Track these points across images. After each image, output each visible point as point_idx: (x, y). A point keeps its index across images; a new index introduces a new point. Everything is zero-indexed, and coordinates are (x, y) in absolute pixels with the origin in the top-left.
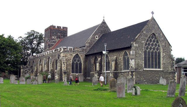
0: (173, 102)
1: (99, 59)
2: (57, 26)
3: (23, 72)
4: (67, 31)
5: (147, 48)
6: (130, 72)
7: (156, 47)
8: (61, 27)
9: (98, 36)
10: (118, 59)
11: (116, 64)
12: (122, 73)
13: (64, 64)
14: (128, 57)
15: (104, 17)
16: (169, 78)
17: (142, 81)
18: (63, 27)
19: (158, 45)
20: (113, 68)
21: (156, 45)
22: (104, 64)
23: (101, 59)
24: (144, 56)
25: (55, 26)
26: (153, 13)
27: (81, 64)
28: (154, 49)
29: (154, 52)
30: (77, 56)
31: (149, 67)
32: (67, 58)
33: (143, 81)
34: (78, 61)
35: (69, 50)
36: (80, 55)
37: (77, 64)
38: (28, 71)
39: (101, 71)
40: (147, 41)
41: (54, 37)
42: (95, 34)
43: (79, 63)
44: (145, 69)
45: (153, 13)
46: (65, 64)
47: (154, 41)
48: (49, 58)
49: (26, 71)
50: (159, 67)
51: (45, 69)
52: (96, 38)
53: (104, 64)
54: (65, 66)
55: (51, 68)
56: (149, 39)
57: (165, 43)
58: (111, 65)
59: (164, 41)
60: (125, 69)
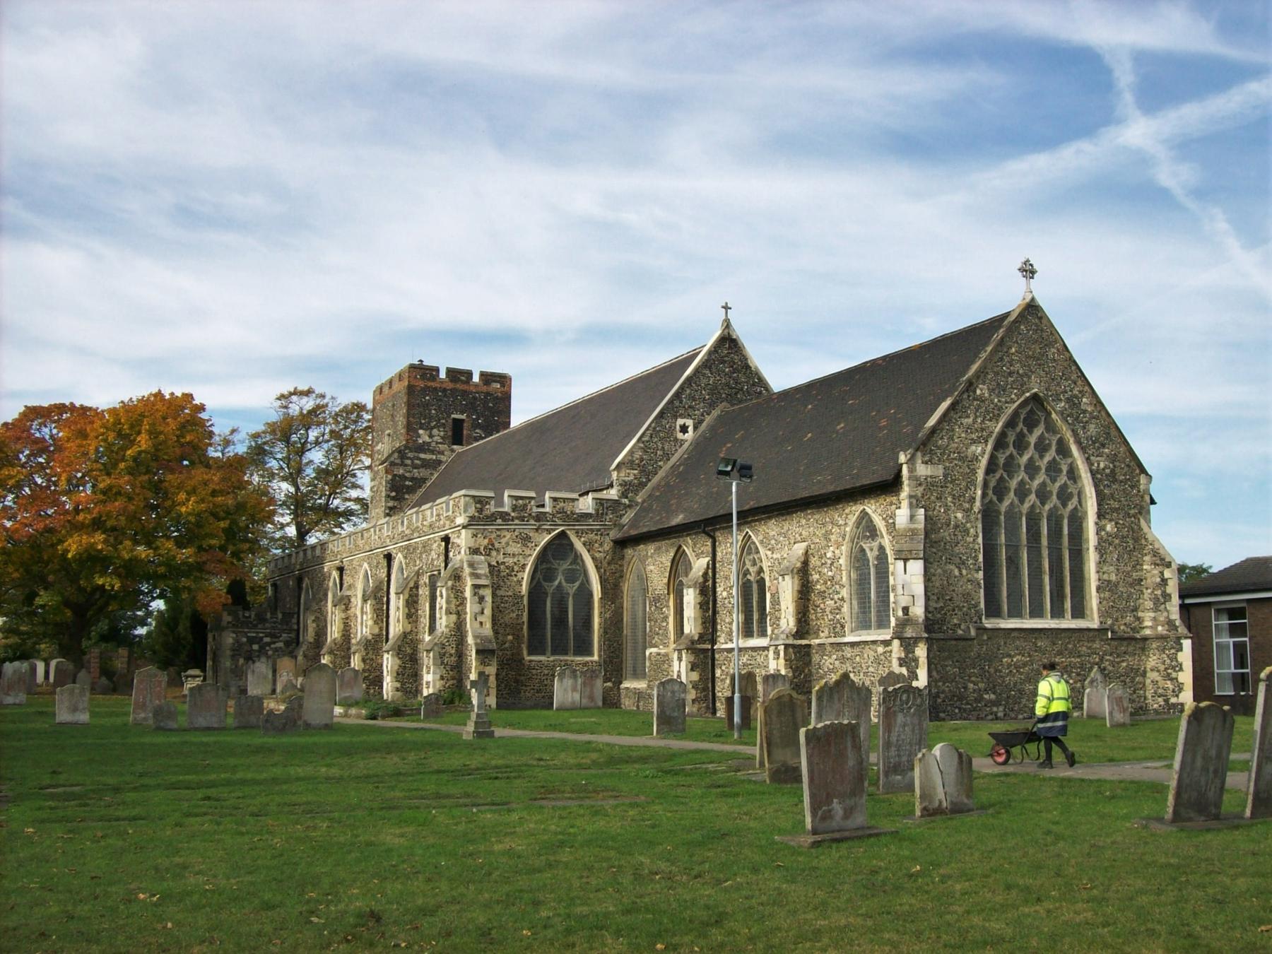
1: (699, 564)
3: (237, 651)
4: (506, 398)
6: (896, 643)
7: (1054, 481)
9: (689, 422)
10: (814, 561)
11: (805, 593)
12: (848, 652)
14: (881, 548)
16: (1144, 674)
17: (976, 700)
18: (483, 374)
19: (1065, 468)
20: (788, 621)
21: (1053, 469)
22: (728, 592)
23: (713, 565)
24: (980, 540)
25: (437, 370)
26: (1028, 271)
27: (585, 594)
28: (1043, 495)
29: (1024, 512)
30: (560, 546)
32: (496, 558)
33: (982, 698)
34: (571, 577)
35: (514, 508)
36: (578, 545)
38: (267, 640)
39: (714, 642)
40: (1000, 444)
41: (431, 436)
42: (671, 411)
43: (572, 589)
44: (989, 623)
46: (489, 599)
48: (389, 558)
49: (251, 641)
50: (1079, 611)
51: (364, 627)
52: (680, 436)
53: (728, 592)
54: (488, 612)
55: (396, 627)
56: (1011, 438)
57: (1113, 458)
58: (776, 602)
59: (1103, 446)
60: (864, 625)
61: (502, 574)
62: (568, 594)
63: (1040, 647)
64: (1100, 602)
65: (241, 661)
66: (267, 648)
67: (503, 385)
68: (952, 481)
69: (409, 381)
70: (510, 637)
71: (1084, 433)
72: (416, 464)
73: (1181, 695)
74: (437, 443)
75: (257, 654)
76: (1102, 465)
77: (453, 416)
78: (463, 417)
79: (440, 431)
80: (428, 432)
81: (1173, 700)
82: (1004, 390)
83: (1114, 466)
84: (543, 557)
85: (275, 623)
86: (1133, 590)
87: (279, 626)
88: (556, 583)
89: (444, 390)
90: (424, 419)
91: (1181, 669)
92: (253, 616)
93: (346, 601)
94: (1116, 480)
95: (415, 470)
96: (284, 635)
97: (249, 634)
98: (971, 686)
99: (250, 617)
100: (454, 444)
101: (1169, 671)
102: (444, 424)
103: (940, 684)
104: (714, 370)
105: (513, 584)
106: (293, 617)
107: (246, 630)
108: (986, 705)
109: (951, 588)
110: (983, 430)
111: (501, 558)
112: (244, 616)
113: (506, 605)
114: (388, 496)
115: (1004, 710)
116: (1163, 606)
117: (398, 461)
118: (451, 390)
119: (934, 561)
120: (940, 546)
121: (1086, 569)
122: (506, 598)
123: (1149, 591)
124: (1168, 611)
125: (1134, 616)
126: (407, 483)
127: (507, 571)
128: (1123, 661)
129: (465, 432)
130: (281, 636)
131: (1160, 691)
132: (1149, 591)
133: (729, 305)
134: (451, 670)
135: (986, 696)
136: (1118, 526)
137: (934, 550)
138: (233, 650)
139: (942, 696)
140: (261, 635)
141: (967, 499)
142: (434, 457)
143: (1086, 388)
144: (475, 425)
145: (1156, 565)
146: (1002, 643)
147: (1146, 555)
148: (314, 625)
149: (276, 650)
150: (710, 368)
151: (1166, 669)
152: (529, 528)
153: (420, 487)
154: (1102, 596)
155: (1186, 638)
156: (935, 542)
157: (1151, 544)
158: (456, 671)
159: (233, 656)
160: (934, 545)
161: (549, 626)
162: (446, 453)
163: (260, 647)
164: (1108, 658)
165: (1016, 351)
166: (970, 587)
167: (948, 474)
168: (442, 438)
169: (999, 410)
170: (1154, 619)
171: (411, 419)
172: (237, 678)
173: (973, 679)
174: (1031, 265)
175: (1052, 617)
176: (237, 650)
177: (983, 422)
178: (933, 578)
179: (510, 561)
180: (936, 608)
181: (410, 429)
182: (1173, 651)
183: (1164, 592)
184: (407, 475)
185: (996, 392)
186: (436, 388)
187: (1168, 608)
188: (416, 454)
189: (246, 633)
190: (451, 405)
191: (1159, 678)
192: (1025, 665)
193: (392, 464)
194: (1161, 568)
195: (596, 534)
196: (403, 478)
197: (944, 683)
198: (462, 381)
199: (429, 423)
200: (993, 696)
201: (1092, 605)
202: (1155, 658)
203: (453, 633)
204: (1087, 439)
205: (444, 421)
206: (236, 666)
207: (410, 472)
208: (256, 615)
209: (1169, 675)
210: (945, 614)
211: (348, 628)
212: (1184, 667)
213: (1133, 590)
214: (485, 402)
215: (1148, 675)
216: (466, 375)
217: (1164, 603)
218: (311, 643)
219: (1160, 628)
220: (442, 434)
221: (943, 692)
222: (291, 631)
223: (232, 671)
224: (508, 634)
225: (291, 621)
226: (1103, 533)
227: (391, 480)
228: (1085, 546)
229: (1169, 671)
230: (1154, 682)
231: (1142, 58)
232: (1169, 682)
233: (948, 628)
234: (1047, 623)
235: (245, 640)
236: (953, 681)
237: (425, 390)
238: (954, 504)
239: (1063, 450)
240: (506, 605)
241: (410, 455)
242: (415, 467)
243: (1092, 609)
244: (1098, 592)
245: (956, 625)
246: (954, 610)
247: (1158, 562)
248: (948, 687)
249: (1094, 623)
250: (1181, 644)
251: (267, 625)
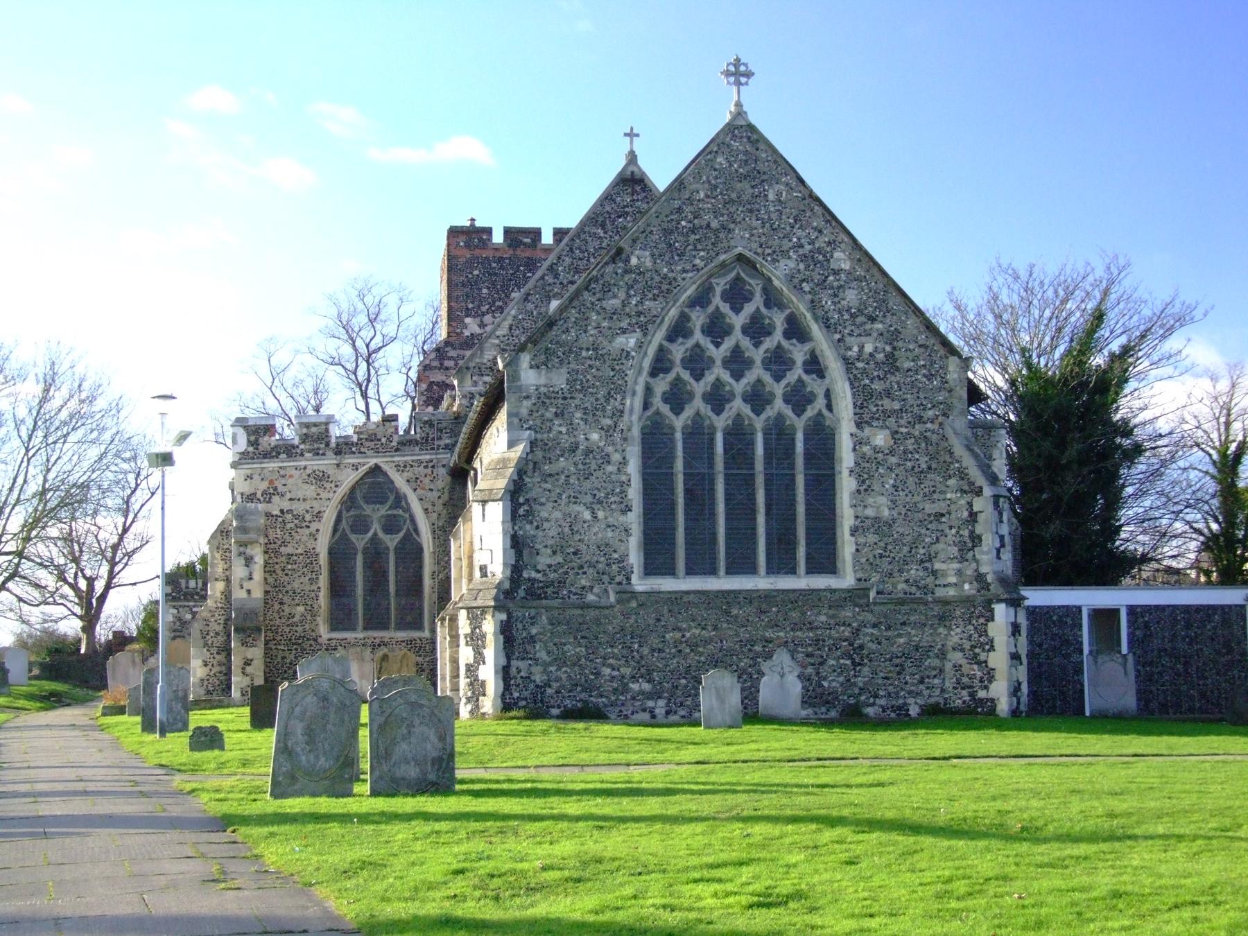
0: (229, 913)
2: (508, 231)
5: (677, 398)
8: (536, 233)
13: (249, 561)
15: (631, 135)
16: (942, 655)
25: (488, 231)
31: (701, 564)
32: (276, 505)
33: (625, 689)
36: (399, 481)
37: (375, 555)
41: (482, 325)
43: (391, 541)
45: (738, 73)
46: (259, 559)
47: (757, 329)
50: (824, 561)
54: (258, 575)
57: (893, 337)
59: (873, 319)
61: (289, 526)
62: (388, 548)
63: (736, 617)
64: (857, 550)
68: (583, 390)
70: (301, 609)
71: (834, 303)
73: (993, 686)
76: (869, 348)
80: (478, 320)
81: (982, 694)
82: (680, 255)
83: (894, 348)
84: (350, 501)
86: (923, 531)
88: (370, 534)
90: (473, 303)
91: (992, 648)
94: (898, 369)
98: (607, 671)
101: (977, 650)
103: (553, 669)
104: (609, 226)
105: (305, 538)
107: (191, 604)
108: (633, 698)
109: (577, 537)
110: (639, 314)
111: (286, 505)
113: (294, 567)
115: (667, 705)
116: (970, 554)
117: (436, 364)
119: (548, 500)
120: (557, 480)
121: (838, 502)
122: (295, 558)
123: (954, 531)
124: (977, 561)
125: (926, 569)
127: (296, 521)
128: (900, 636)
131: (965, 680)
132: (954, 531)
133: (635, 131)
134: (218, 653)
135: (634, 686)
136: (897, 436)
137: (548, 486)
139: (555, 685)
141: (609, 413)
143: (843, 236)
145: (963, 492)
146: (665, 611)
147: (950, 477)
150: (603, 226)
151: (973, 647)
152: (326, 463)
154: (862, 540)
155: (1000, 601)
156: (550, 475)
157: (958, 461)
158: (224, 654)
160: (548, 479)
161: (360, 591)
164: (870, 630)
165: (707, 196)
166: (610, 534)
167: (575, 380)
169: (670, 283)
170: (959, 573)
171: (452, 304)
173: (611, 661)
174: (746, 65)
176: (178, 631)
177: (641, 302)
178: (546, 525)
179: (299, 508)
180: (550, 566)
182: (982, 620)
183: (972, 532)
185: (667, 258)
186: (487, 258)
187: (977, 557)
191: (963, 662)
192: (706, 642)
194: (968, 497)
195: (426, 467)
197: (559, 669)
198: (525, 244)
199: (479, 307)
200: (646, 687)
201: (844, 557)
202: (958, 630)
203: (220, 605)
204: (840, 312)
209: (976, 655)
210: (567, 573)
212: (996, 644)
213: (923, 531)
215: (949, 656)
217: (972, 549)
219: (967, 586)
221: (558, 679)
224: (298, 605)
226: (866, 449)
228: (837, 468)
229: (977, 650)
230: (958, 667)
232: (975, 667)
233: (570, 592)
234: (761, 582)
236: (574, 665)
238: (586, 421)
239: (795, 330)
240: (294, 567)
243: (844, 561)
244: (852, 535)
245: (583, 588)
246: (581, 567)
247: (966, 488)
248: (566, 672)
249: (846, 580)
250: (992, 611)
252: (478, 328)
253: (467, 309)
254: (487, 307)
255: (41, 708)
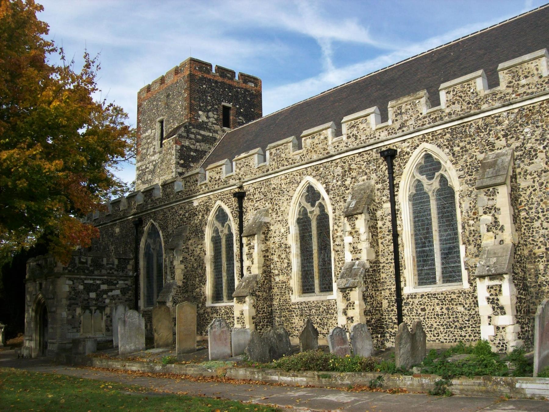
8: (233, 73)
38: (104, 287)
41: (208, 117)
49: (89, 288)
65: (79, 311)
66: (105, 296)
67: (256, 85)
69: (190, 71)
72: (198, 139)
74: (213, 124)
75: (94, 302)
77: (223, 104)
78: (230, 105)
79: (214, 114)
85: (111, 269)
87: (116, 273)
89: (216, 82)
92: (89, 262)
93: (264, 229)
95: (197, 144)
96: (120, 282)
97: (86, 282)
99: (86, 263)
100: (224, 126)
102: (216, 109)
106: (128, 263)
112: (81, 262)
114: (178, 163)
117: (185, 134)
118: (221, 83)
126: (192, 153)
129: (231, 118)
130: (117, 283)
138: (70, 299)
140: (98, 282)
142: (211, 135)
144: (238, 114)
148: (182, 266)
149: (113, 298)
153: (202, 158)
159: (70, 306)
162: (219, 132)
163: (97, 295)
168: (216, 120)
171: (193, 101)
172: (75, 330)
175: (444, 282)
181: (192, 109)
184: (192, 146)
186: (210, 80)
188: (198, 131)
189: (83, 280)
190: (221, 95)
193: (180, 136)
196: (188, 148)
198: (228, 77)
199: (206, 106)
205: (217, 107)
206: (73, 317)
207: (194, 145)
208: (92, 261)
211: (268, 263)
214: (245, 97)
216: (231, 73)
218: (179, 287)
220: (216, 116)
222: (126, 278)
223: (69, 322)
225: (126, 267)
227: (180, 150)
231: (336, 43)
235: (81, 287)
237: (202, 79)
241: (193, 130)
242: (198, 141)
251: (104, 272)
252: (205, 119)
253: (200, 106)
254: (210, 107)
255: (116, 310)
